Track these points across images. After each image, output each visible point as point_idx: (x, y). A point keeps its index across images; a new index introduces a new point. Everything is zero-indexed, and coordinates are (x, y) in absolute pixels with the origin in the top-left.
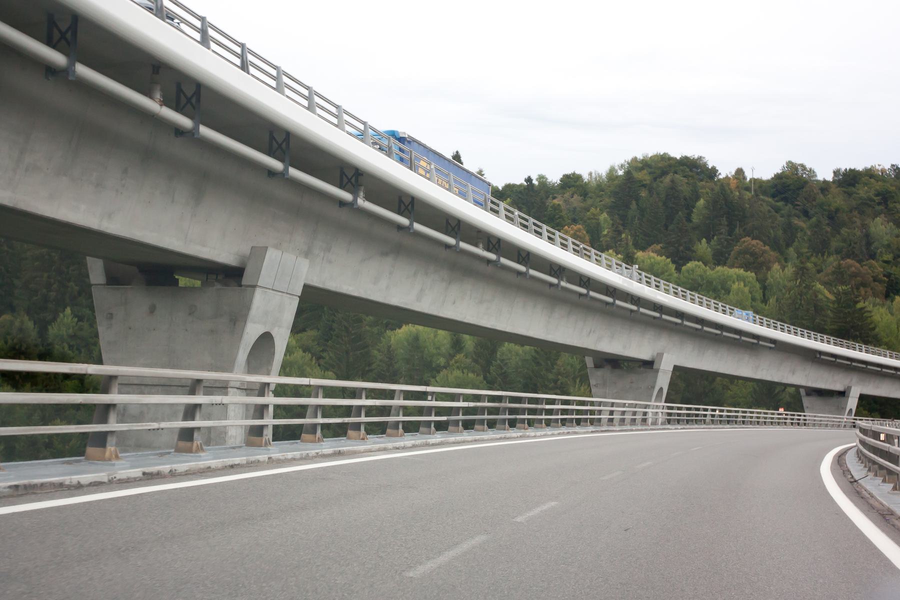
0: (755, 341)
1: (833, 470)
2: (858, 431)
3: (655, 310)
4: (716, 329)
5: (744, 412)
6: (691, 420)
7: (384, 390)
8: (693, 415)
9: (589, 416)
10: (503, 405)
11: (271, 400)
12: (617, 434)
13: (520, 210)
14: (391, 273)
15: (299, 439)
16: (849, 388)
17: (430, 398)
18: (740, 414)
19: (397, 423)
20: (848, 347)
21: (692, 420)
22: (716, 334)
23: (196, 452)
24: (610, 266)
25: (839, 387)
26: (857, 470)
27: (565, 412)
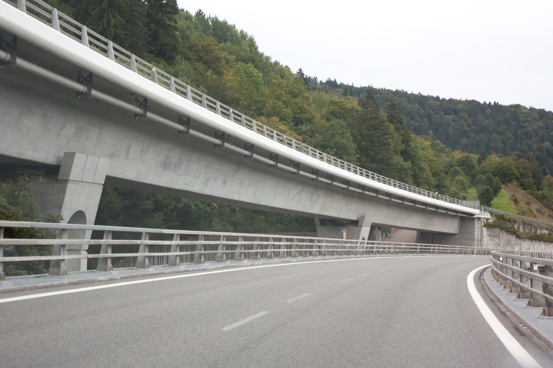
0: (445, 212)
1: (475, 277)
2: (491, 257)
3: (344, 184)
4: (359, 188)
5: (438, 247)
6: (422, 251)
7: (248, 237)
8: (423, 249)
9: (308, 250)
10: (294, 243)
11: (437, 248)
12: (330, 260)
13: (246, 114)
14: (142, 151)
15: (96, 268)
16: (363, 217)
17: (240, 239)
18: (418, 247)
19: (257, 253)
20: (384, 182)
21: (423, 252)
22: (400, 203)
23: (63, 275)
24: (315, 155)
25: (354, 217)
26: (488, 278)
27: (425, 249)
